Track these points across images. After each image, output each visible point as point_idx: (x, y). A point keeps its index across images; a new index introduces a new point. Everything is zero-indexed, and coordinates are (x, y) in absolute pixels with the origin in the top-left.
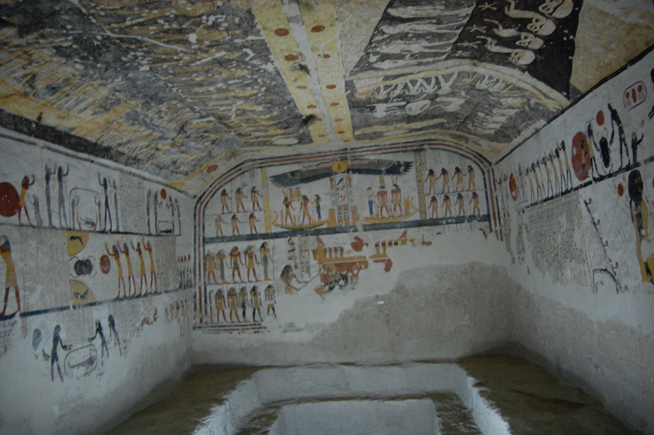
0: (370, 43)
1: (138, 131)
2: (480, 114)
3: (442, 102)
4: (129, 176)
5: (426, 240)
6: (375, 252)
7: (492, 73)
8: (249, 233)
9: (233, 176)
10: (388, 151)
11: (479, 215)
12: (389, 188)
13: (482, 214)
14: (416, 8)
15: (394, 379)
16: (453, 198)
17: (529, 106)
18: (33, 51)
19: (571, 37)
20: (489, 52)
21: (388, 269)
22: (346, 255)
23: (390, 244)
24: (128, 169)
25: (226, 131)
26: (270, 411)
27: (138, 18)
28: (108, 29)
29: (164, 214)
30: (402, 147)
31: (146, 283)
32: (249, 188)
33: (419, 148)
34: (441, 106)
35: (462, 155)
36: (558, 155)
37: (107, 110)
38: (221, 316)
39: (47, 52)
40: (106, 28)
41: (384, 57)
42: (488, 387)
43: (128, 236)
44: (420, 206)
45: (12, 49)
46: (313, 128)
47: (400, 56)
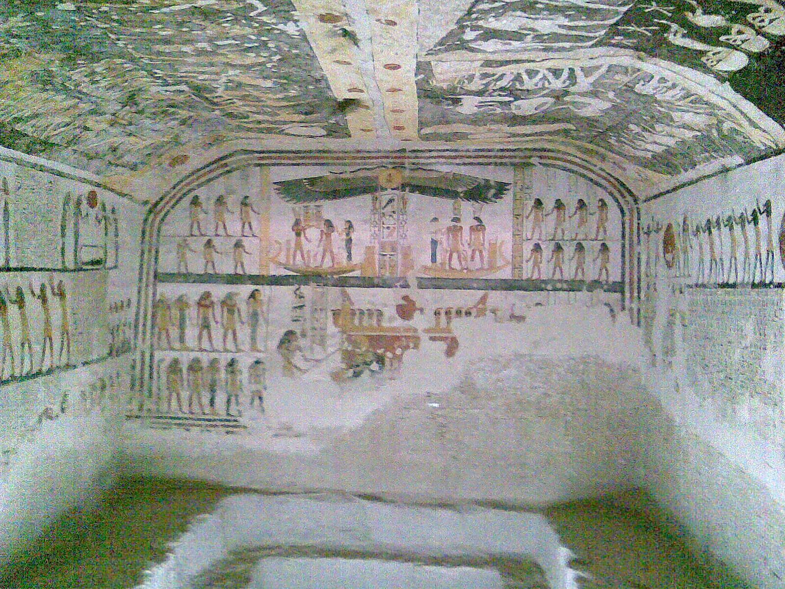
0: (470, 13)
1: (52, 101)
2: (631, 126)
3: (574, 103)
4: (33, 172)
5: (517, 313)
6: (433, 324)
8: (232, 272)
9: (212, 175)
10: (471, 160)
11: (607, 282)
12: (467, 222)
13: (611, 280)
15: (442, 530)
16: (569, 250)
17: (719, 131)
20: (669, 44)
21: (450, 352)
22: (385, 324)
23: (459, 313)
24: (33, 159)
26: (240, 568)
29: (91, 233)
30: (495, 157)
31: (51, 349)
32: (238, 197)
34: (571, 107)
35: (591, 180)
36: (755, 220)
38: (174, 403)
41: (490, 34)
42: (588, 570)
43: (25, 274)
44: (513, 257)
46: (352, 118)
47: (518, 36)
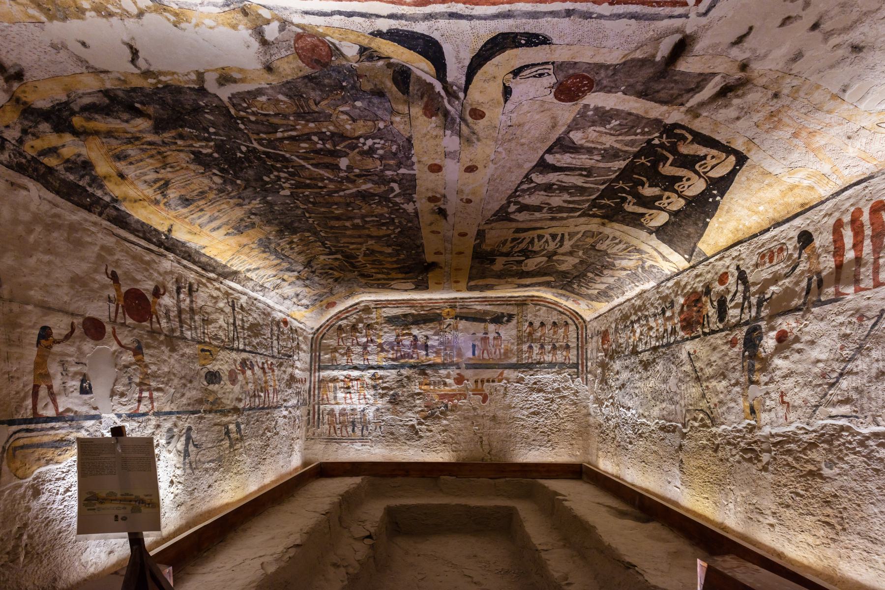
0: (516, 191)
7: (618, 234)
14: (573, 156)
18: (168, 153)
19: (718, 198)
20: (625, 211)
23: (488, 381)
25: (350, 271)
27: (291, 130)
28: (255, 140)
39: (184, 157)
40: (253, 137)
45: (145, 146)
47: (539, 209)
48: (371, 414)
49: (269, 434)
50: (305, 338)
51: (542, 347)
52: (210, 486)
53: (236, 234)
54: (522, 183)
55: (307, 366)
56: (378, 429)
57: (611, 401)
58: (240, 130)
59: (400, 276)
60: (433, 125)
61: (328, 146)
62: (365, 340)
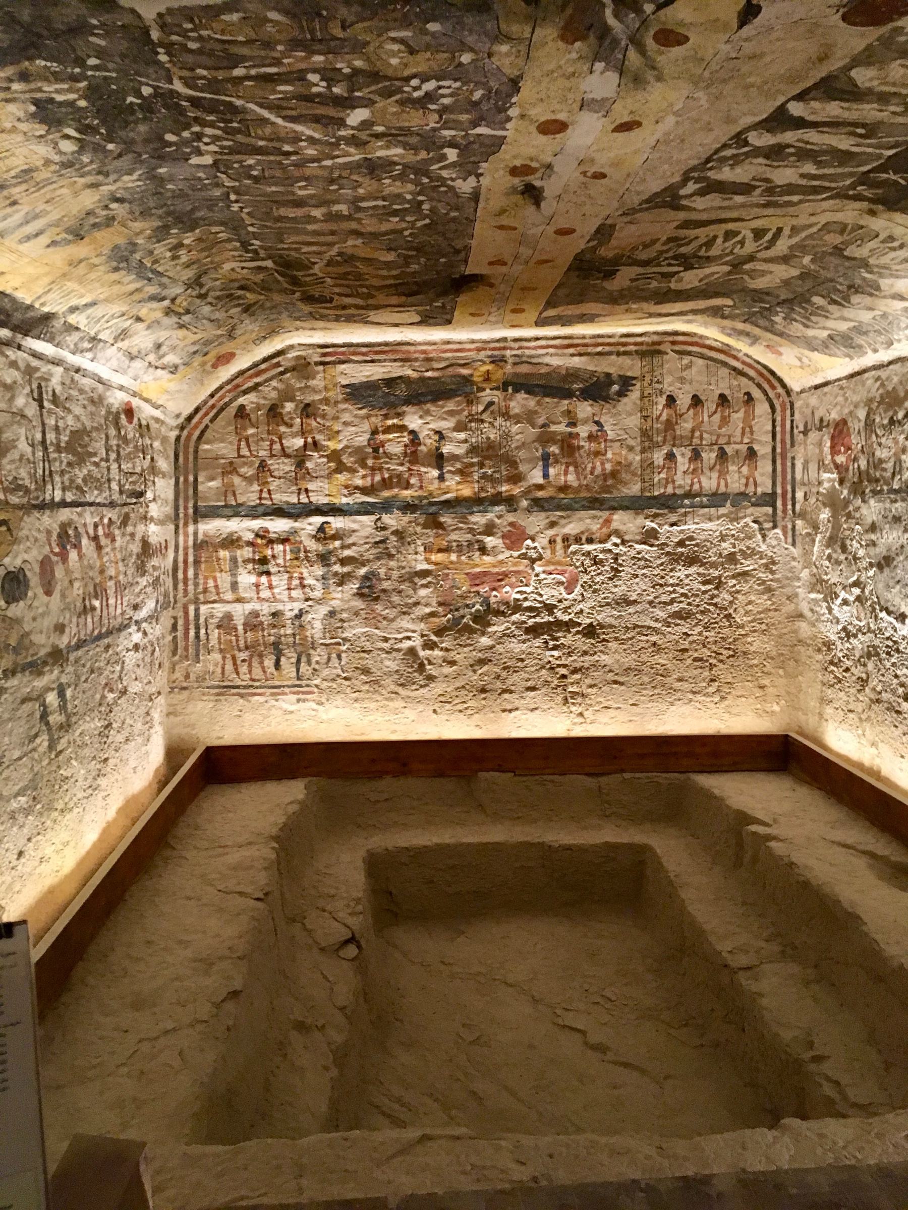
0: (708, 160)
13: (759, 490)
23: (578, 540)
25: (284, 291)
28: (181, 78)
33: (652, 348)
35: (734, 369)
37: (79, 236)
47: (745, 189)
48: (318, 625)
49: (111, 696)
50: (164, 440)
51: (696, 455)
52: (20, 854)
53: (69, 242)
54: (725, 146)
55: (169, 509)
56: (335, 661)
57: (857, 591)
58: (159, 63)
59: (394, 300)
60: (574, 55)
61: (336, 90)
62: (299, 442)
